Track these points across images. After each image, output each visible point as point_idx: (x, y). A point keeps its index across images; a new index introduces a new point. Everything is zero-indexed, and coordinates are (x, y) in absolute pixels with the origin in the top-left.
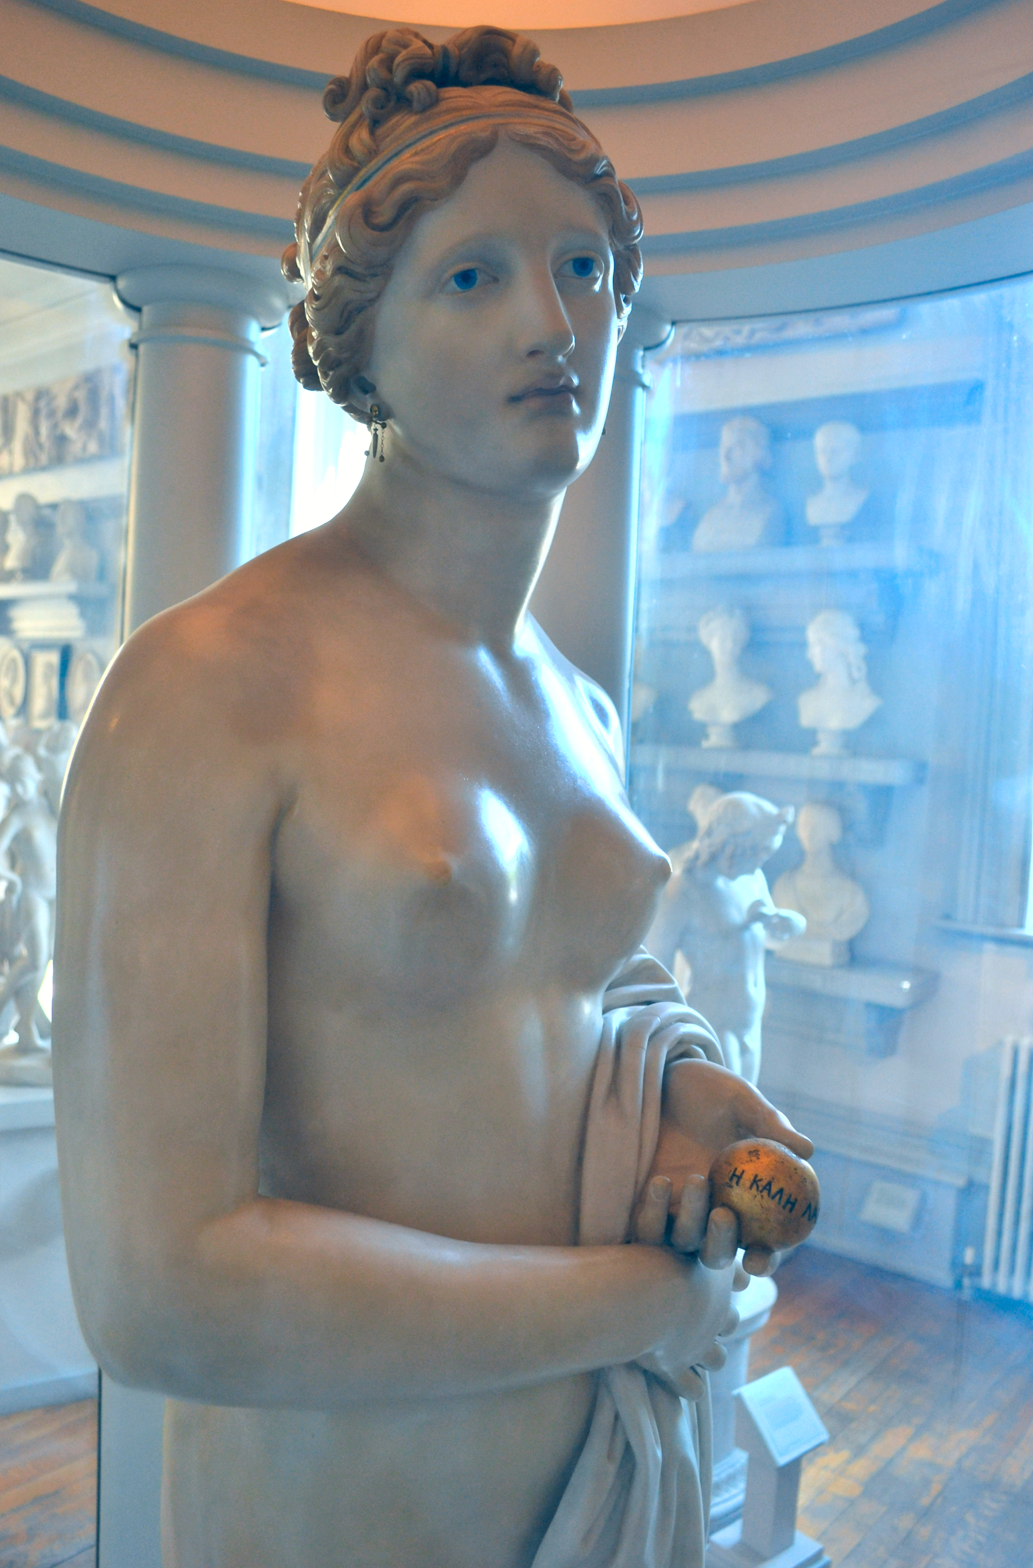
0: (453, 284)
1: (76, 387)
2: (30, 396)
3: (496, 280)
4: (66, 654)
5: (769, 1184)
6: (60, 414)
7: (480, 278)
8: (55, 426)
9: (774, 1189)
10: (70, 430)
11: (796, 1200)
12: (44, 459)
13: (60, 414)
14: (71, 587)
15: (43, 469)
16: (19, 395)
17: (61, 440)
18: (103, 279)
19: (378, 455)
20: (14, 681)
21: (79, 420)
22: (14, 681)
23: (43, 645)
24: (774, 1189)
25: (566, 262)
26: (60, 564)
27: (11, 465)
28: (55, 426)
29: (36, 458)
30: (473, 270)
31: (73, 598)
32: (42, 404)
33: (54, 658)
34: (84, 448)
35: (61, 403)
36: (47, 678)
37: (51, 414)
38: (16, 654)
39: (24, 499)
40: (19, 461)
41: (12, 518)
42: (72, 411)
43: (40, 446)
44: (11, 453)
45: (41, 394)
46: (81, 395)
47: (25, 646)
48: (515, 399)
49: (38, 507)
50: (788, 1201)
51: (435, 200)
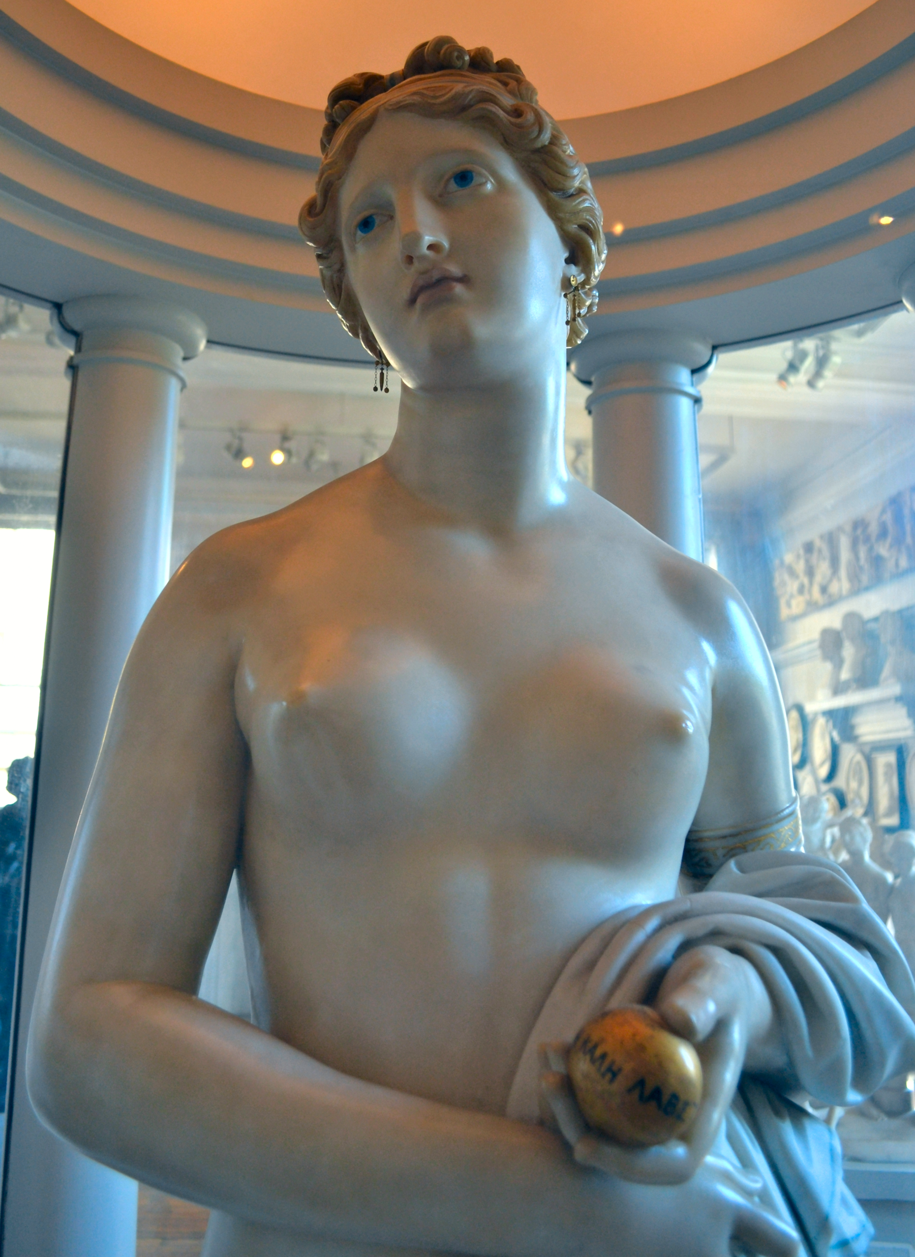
0: (359, 233)
1: (883, 511)
2: (848, 528)
3: (392, 217)
4: (901, 751)
5: (595, 1047)
6: (873, 538)
7: (377, 221)
8: (871, 549)
9: (598, 1052)
10: (883, 550)
11: (620, 1070)
12: (865, 579)
13: (873, 538)
14: (895, 689)
15: (867, 589)
16: (840, 529)
17: (877, 561)
18: (44, 303)
19: (384, 388)
20: (860, 783)
21: (889, 540)
22: (860, 783)
23: (880, 747)
24: (598, 1052)
25: (448, 180)
26: (887, 671)
27: (840, 590)
28: (871, 549)
29: (859, 581)
30: (370, 217)
31: (898, 699)
32: (859, 531)
33: (891, 758)
34: (897, 565)
35: (874, 529)
36: (887, 775)
37: (867, 539)
38: (859, 757)
39: (850, 617)
40: (845, 585)
41: (844, 635)
42: (883, 533)
43: (861, 568)
44: (839, 580)
45: (859, 525)
46: (888, 517)
47: (867, 749)
48: (412, 301)
49: (864, 623)
50: (609, 1069)
51: (340, 178)
